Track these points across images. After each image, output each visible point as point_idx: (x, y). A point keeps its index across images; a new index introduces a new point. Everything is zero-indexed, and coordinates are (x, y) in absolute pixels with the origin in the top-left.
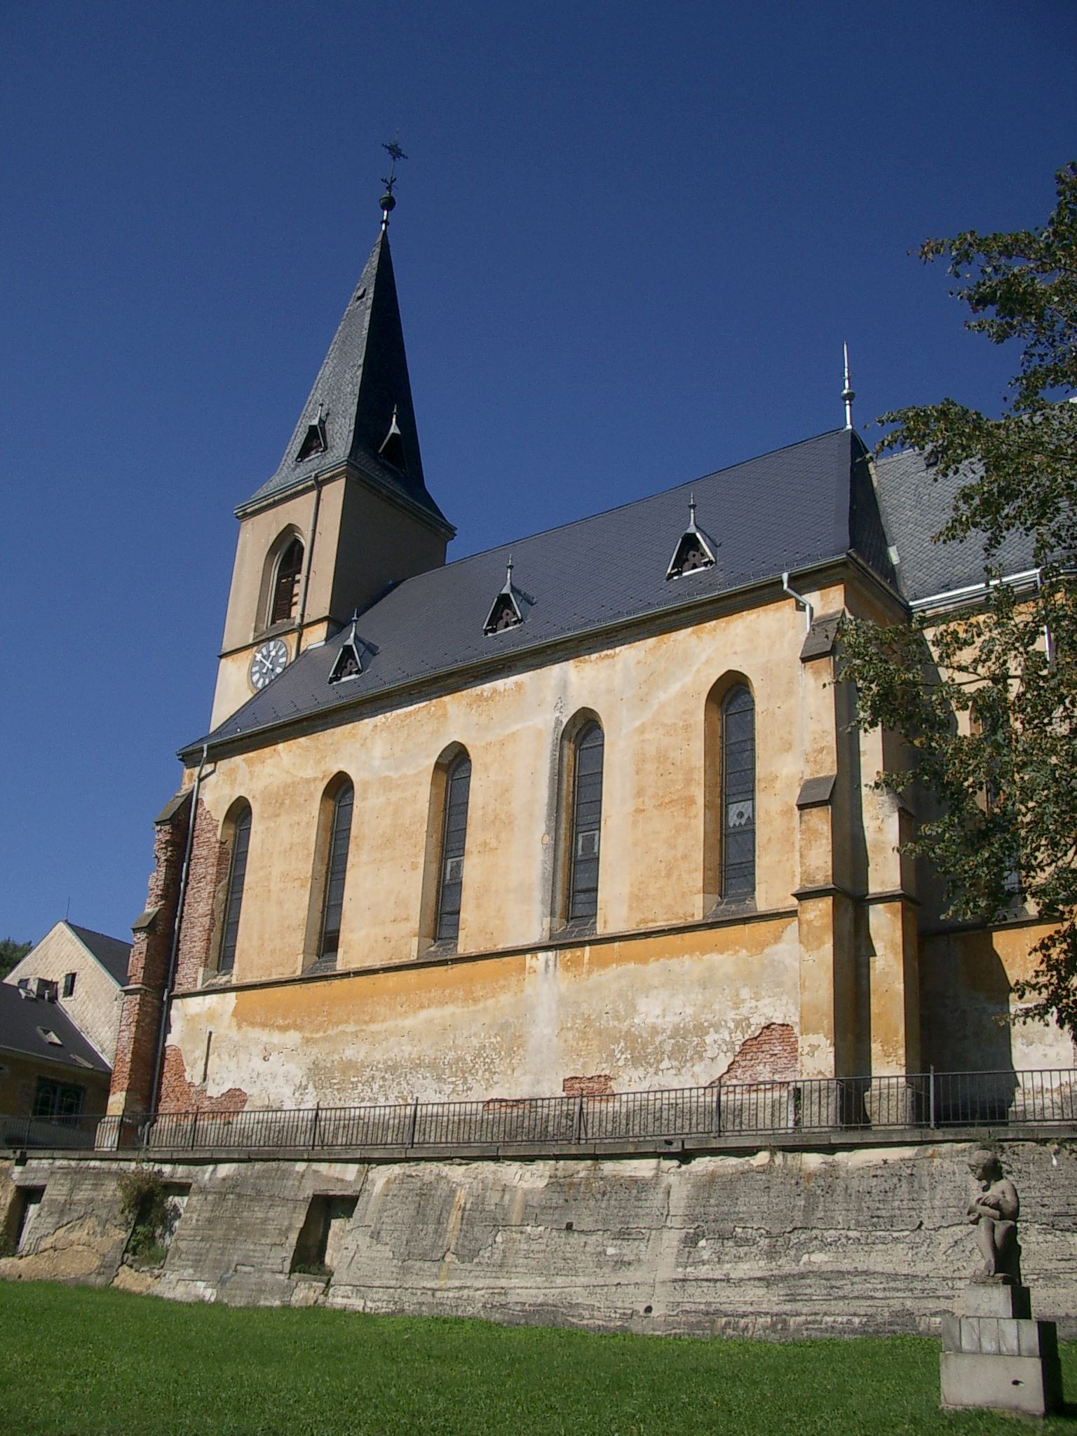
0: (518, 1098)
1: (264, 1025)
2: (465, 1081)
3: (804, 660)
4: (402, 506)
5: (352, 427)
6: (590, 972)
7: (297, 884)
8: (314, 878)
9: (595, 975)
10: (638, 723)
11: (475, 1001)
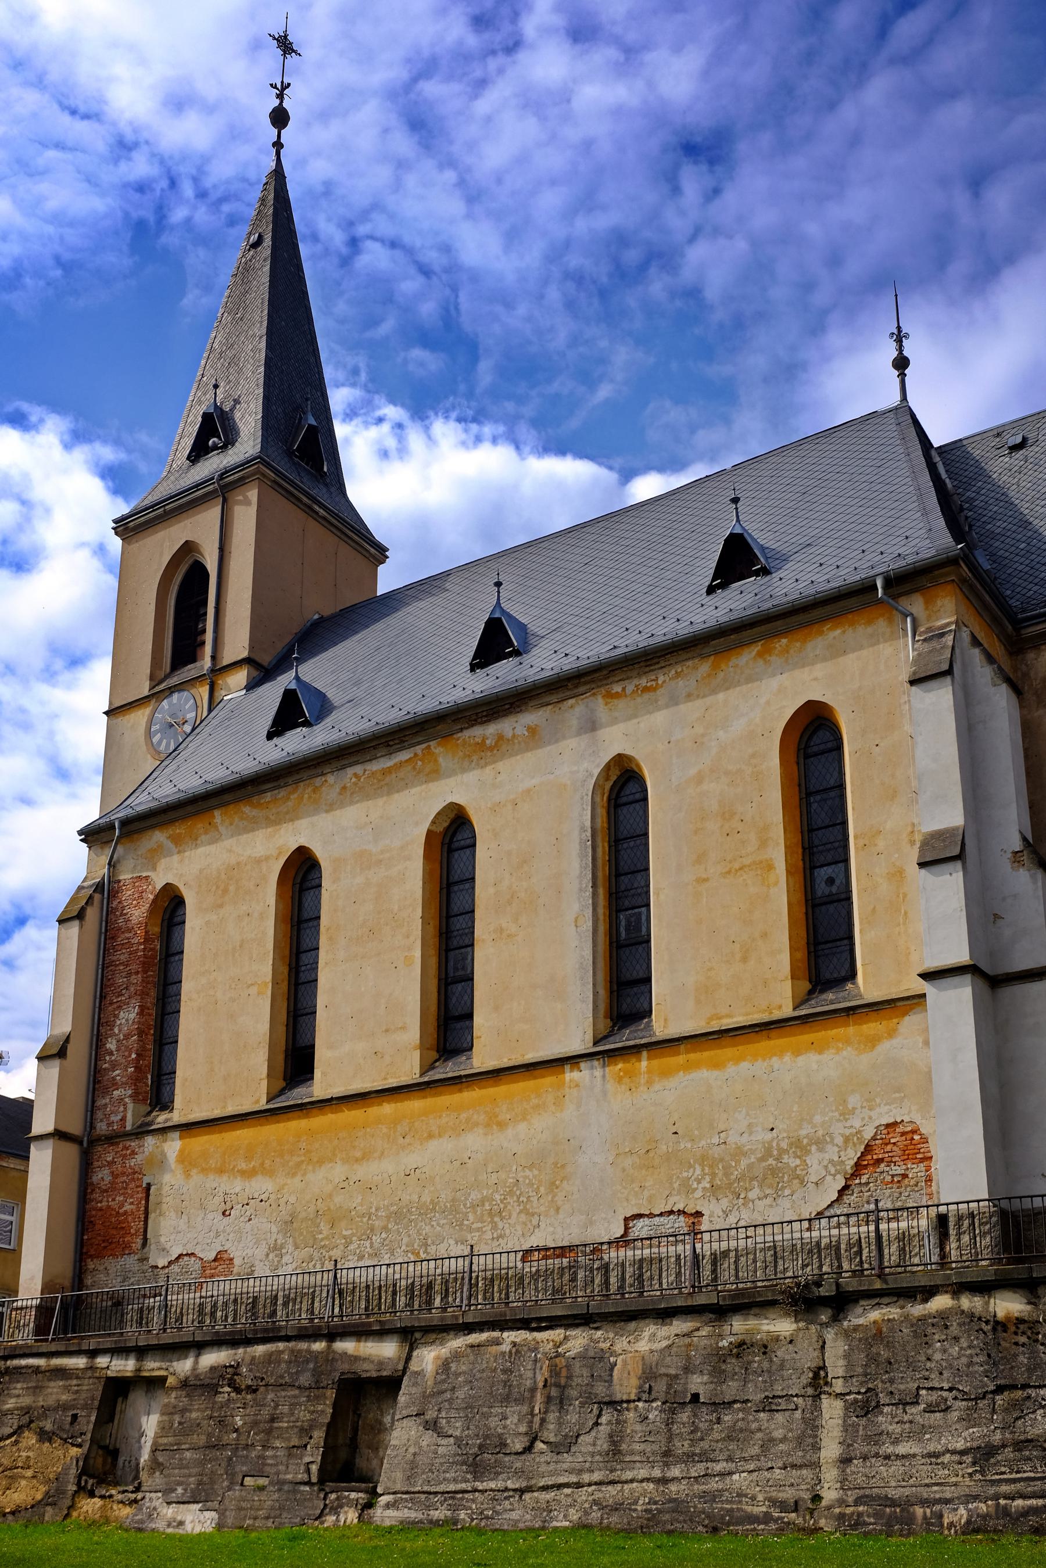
0: (565, 1243)
1: (221, 1171)
2: (495, 1227)
3: (912, 683)
4: (324, 518)
5: (260, 416)
6: (649, 1083)
7: (253, 990)
8: (275, 983)
9: (657, 1086)
10: (693, 771)
11: (502, 1125)
